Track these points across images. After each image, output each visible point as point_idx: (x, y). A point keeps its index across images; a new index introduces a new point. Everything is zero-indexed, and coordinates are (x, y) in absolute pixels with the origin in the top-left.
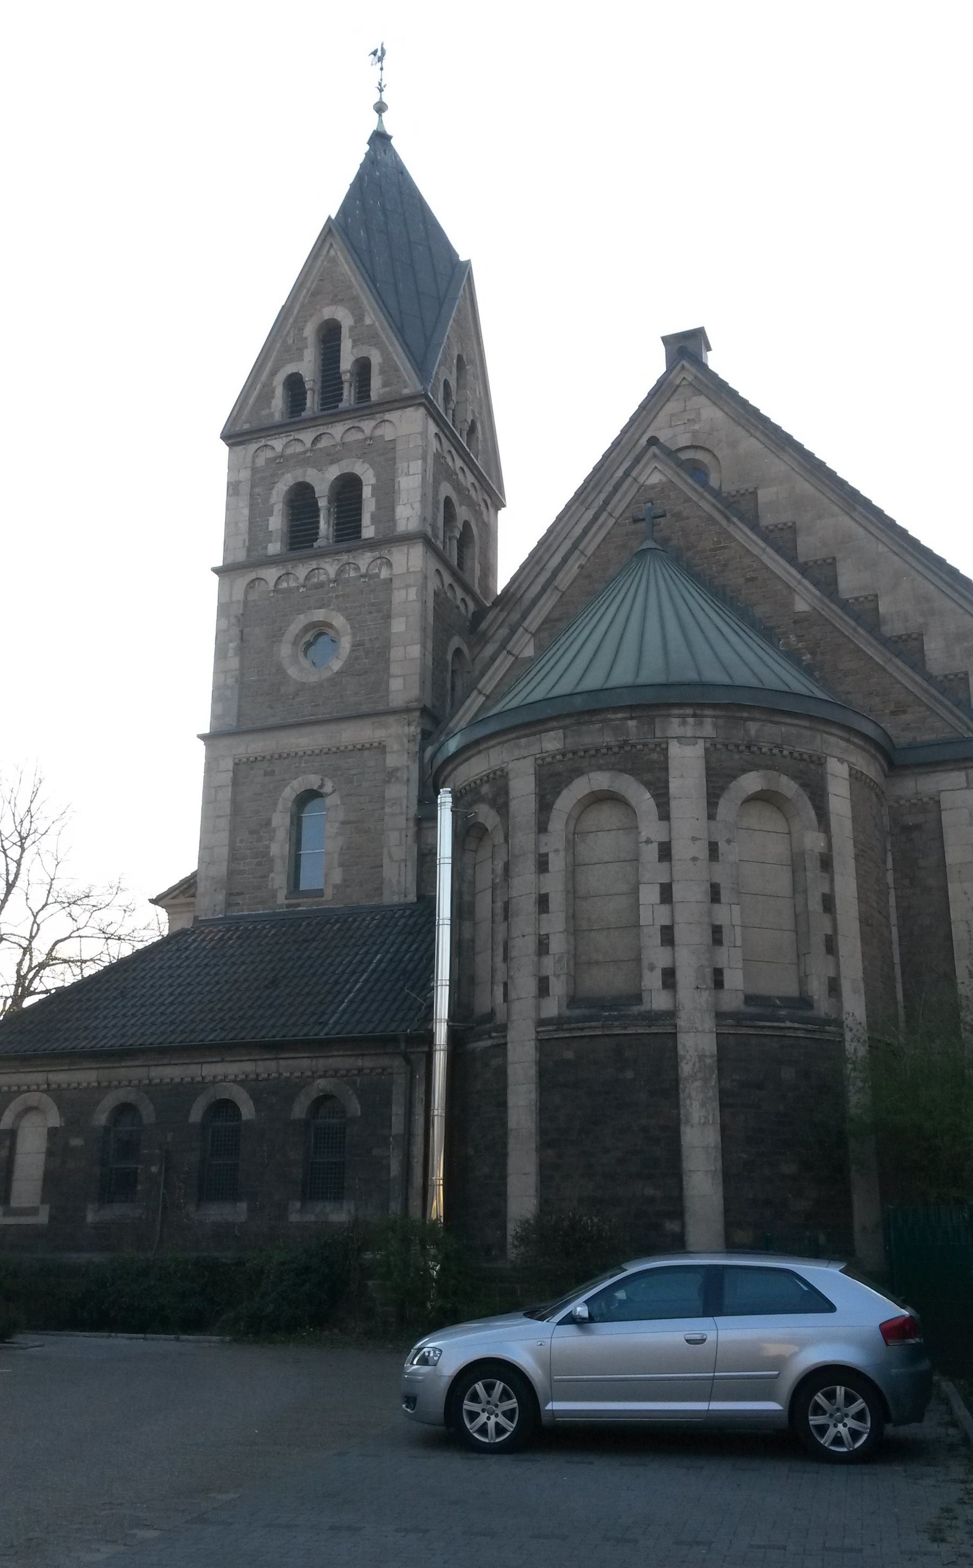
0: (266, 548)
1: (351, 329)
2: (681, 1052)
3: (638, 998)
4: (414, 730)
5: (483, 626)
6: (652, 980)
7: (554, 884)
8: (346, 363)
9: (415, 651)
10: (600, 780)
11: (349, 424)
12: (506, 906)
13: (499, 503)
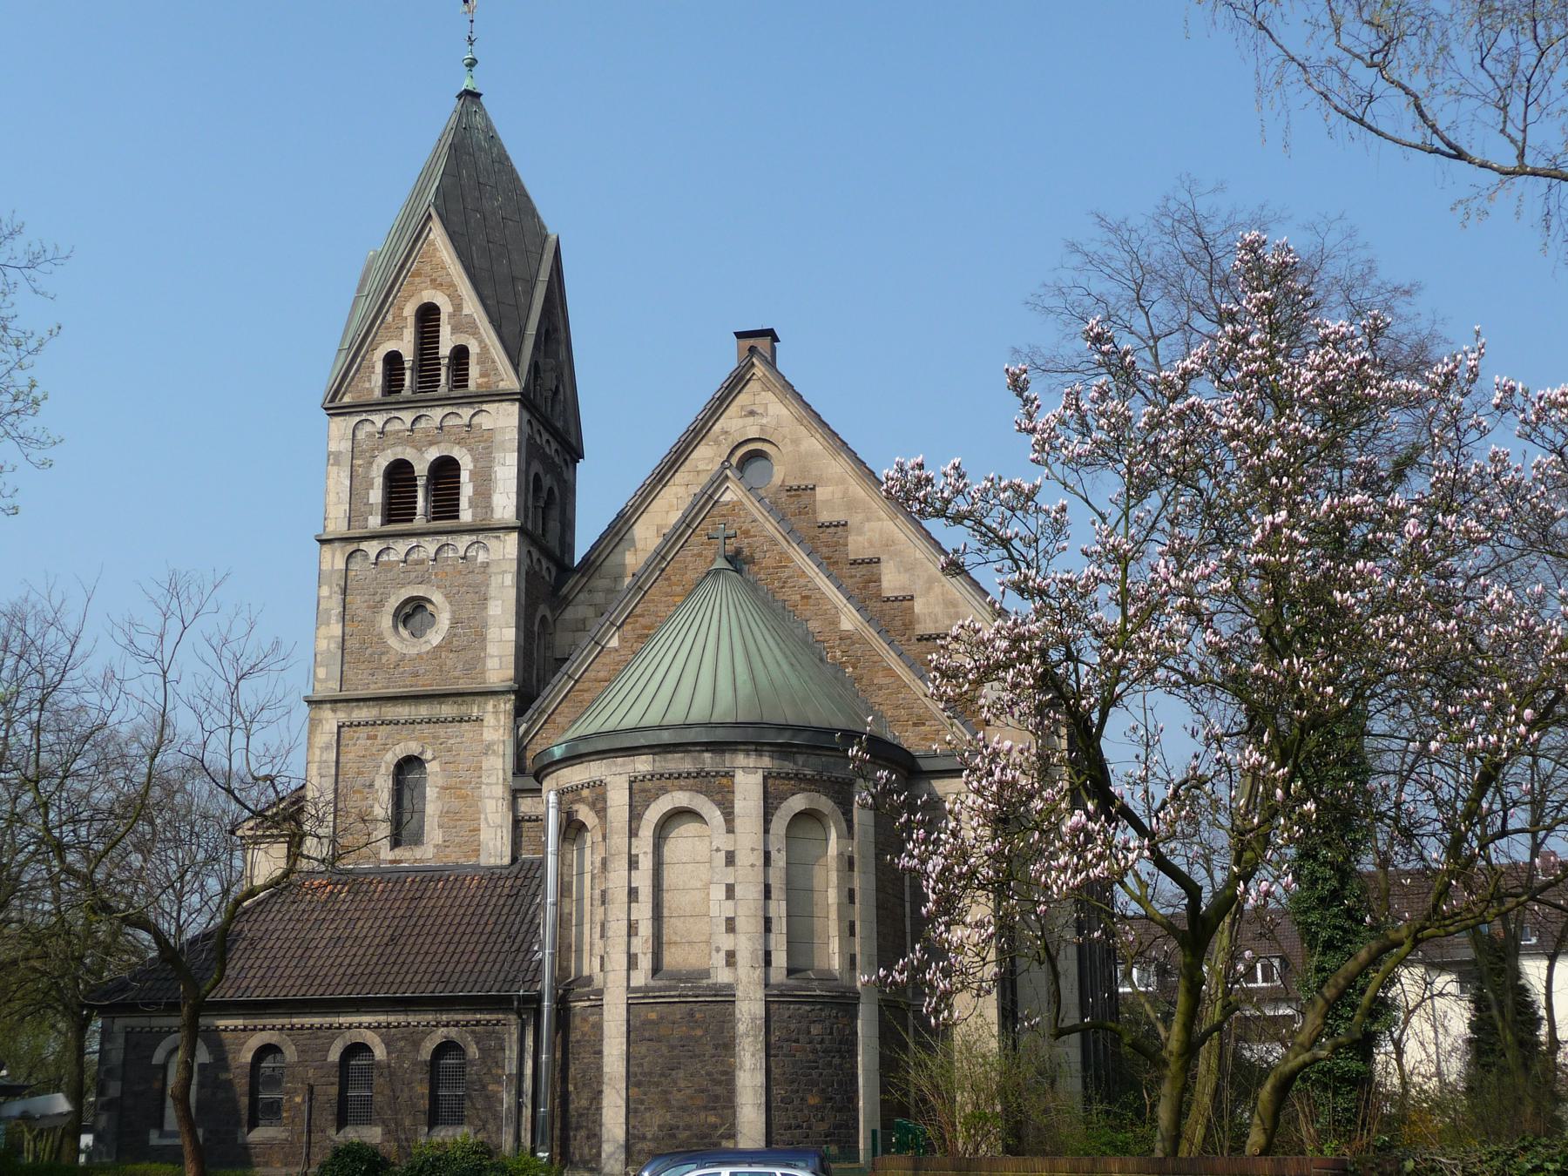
0: (366, 520)
1: (451, 316)
2: (738, 1015)
3: (706, 974)
4: (509, 706)
5: (565, 590)
6: (719, 960)
7: (643, 879)
8: (445, 350)
9: (510, 634)
10: (681, 799)
11: (448, 410)
12: (604, 893)
13: (576, 453)
